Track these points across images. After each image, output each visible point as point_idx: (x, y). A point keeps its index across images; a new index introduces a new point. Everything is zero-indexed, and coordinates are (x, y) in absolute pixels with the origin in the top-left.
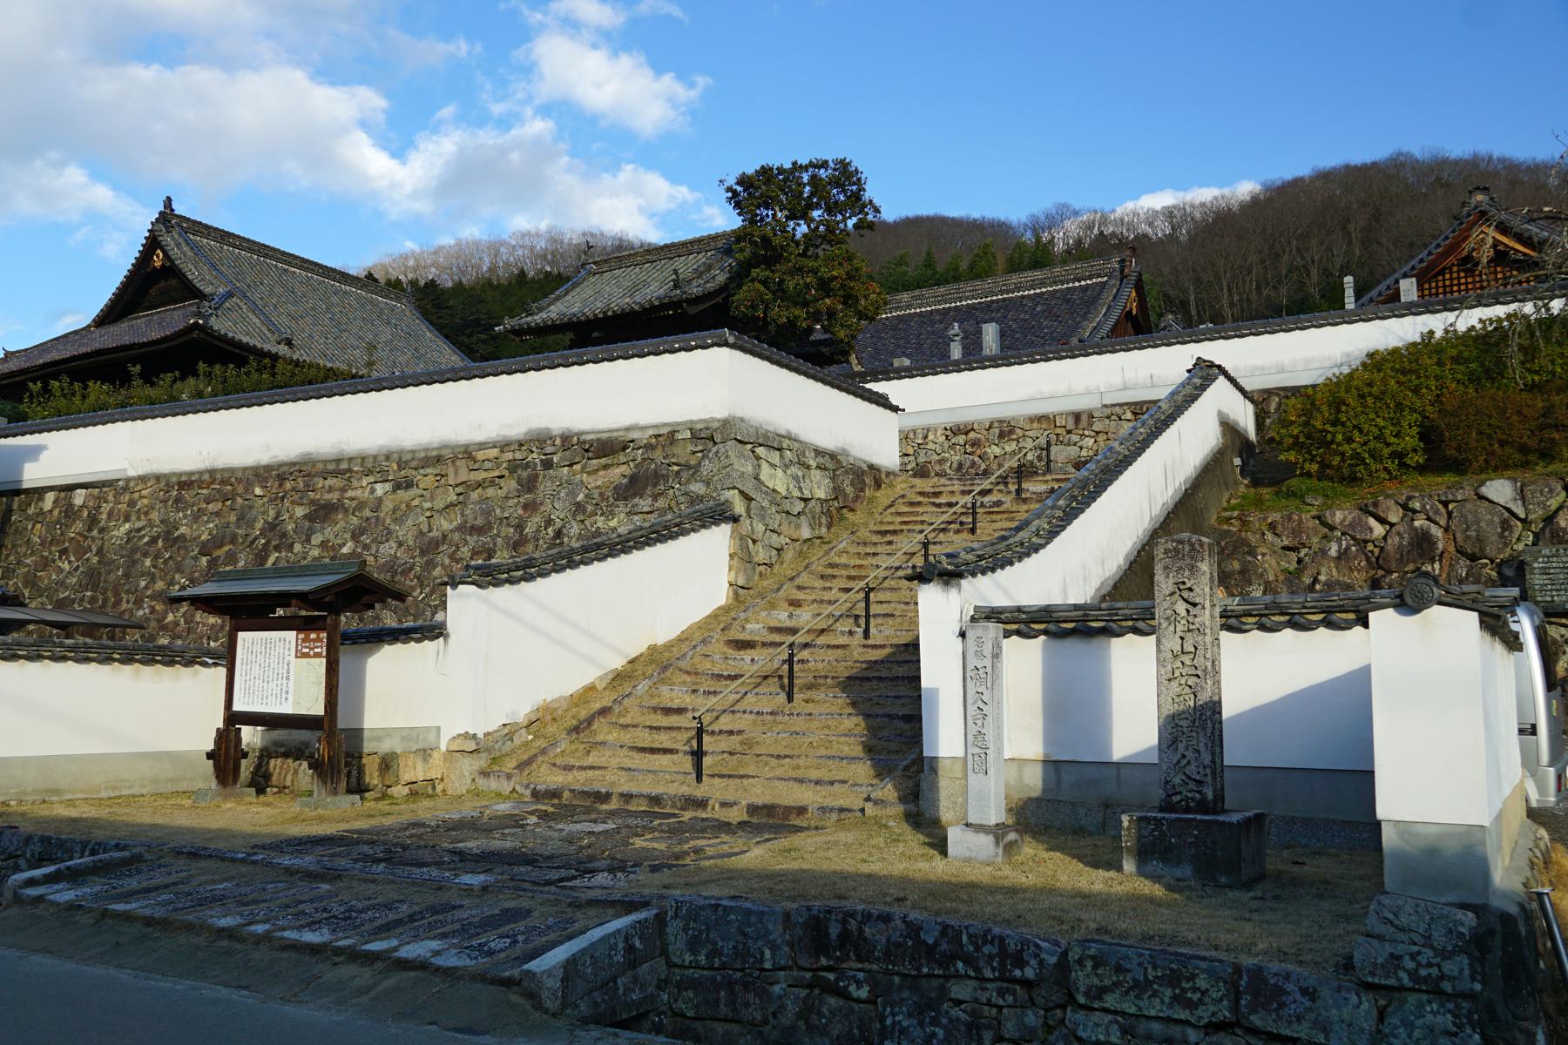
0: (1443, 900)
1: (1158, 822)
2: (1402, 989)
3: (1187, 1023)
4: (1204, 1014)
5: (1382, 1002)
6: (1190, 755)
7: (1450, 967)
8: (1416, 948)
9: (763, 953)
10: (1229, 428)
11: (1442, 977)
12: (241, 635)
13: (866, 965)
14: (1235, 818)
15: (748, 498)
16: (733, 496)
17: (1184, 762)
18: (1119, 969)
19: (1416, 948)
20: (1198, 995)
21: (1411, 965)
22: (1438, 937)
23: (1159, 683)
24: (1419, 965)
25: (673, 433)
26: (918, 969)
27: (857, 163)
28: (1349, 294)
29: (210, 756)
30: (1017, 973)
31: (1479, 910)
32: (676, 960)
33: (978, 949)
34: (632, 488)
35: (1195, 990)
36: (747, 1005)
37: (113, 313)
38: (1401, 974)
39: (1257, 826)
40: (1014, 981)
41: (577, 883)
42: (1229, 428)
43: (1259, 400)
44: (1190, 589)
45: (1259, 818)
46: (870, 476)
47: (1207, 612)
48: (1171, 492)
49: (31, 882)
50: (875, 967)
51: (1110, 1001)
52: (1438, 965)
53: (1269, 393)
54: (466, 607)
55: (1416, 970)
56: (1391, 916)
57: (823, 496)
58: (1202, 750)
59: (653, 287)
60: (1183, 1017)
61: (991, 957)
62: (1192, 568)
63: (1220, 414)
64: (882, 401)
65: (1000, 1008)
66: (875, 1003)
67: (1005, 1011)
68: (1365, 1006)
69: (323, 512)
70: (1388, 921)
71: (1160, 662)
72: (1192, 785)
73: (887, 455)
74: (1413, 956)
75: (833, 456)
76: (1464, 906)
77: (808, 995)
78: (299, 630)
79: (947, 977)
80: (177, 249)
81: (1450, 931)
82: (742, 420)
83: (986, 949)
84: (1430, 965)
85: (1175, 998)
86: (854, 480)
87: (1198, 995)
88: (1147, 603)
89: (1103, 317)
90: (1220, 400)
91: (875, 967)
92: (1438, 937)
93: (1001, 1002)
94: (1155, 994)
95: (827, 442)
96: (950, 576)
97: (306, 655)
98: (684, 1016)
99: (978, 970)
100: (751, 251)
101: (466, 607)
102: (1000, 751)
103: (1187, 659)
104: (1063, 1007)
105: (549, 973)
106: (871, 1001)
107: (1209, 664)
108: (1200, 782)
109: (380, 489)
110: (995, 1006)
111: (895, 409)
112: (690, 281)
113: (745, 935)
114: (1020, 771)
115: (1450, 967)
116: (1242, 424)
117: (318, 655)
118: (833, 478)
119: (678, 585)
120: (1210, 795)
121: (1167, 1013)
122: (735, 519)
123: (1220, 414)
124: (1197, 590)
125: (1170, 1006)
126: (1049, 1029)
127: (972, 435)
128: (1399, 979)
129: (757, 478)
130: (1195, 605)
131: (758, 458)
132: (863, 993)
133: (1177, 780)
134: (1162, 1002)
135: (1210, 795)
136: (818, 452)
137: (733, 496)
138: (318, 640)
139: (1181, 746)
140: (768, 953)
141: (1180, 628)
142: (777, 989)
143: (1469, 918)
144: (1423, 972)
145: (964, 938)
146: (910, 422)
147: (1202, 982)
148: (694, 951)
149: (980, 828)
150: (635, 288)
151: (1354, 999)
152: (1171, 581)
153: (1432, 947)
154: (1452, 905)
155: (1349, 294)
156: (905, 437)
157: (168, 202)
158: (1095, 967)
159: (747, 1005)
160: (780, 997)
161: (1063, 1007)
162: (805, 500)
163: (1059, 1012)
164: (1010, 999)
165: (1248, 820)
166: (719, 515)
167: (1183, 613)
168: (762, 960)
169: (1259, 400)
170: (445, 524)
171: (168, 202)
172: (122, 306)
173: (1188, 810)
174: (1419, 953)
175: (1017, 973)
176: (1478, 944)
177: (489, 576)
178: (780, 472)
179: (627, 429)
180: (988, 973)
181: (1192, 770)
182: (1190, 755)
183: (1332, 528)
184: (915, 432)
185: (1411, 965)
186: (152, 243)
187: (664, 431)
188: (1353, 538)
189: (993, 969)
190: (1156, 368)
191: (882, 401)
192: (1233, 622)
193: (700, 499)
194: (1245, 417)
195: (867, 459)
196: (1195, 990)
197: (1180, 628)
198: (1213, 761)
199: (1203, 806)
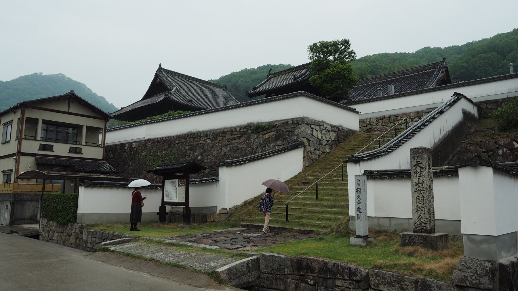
0: (482, 259)
2: (467, 287)
6: (422, 215)
7: (482, 280)
8: (472, 274)
10: (465, 113)
11: (480, 283)
12: (166, 181)
13: (313, 275)
14: (437, 234)
15: (309, 141)
16: (304, 140)
18: (384, 278)
19: (472, 274)
21: (470, 279)
22: (480, 271)
23: (412, 193)
24: (473, 280)
25: (287, 122)
26: (327, 276)
27: (312, 44)
29: (158, 213)
30: (355, 278)
31: (492, 262)
32: (263, 271)
33: (343, 270)
34: (278, 138)
36: (280, 285)
37: (147, 96)
38: (467, 282)
39: (428, 234)
40: (353, 280)
41: (240, 249)
42: (465, 113)
43: (478, 105)
44: (421, 163)
45: (446, 236)
46: (351, 132)
47: (427, 170)
48: (442, 135)
49: (106, 244)
50: (315, 275)
52: (479, 280)
54: (224, 173)
55: (472, 281)
56: (464, 264)
59: (288, 80)
61: (347, 273)
62: (422, 157)
63: (463, 110)
64: (354, 111)
65: (350, 288)
69: (193, 148)
70: (463, 265)
71: (412, 186)
72: (423, 224)
74: (471, 277)
75: (337, 127)
76: (489, 261)
78: (179, 179)
79: (335, 279)
80: (165, 77)
81: (483, 269)
82: (307, 118)
83: (346, 270)
84: (476, 279)
86: (343, 135)
89: (434, 81)
91: (315, 275)
92: (480, 271)
93: (350, 287)
94: (393, 286)
95: (336, 123)
96: (356, 161)
97: (181, 186)
98: (264, 287)
99: (343, 277)
100: (317, 66)
101: (224, 173)
102: (366, 213)
103: (420, 185)
105: (222, 272)
106: (314, 285)
108: (425, 224)
109: (208, 141)
111: (358, 113)
113: (280, 264)
114: (378, 220)
115: (482, 280)
116: (472, 112)
117: (184, 186)
118: (337, 134)
119: (288, 166)
120: (429, 228)
122: (305, 147)
123: (463, 110)
124: (423, 163)
128: (466, 284)
129: (312, 134)
130: (422, 168)
131: (312, 128)
132: (312, 282)
133: (418, 223)
135: (429, 228)
136: (332, 126)
137: (304, 140)
138: (184, 181)
139: (419, 212)
140: (286, 270)
142: (289, 280)
143: (489, 265)
144: (474, 282)
145: (340, 267)
146: (364, 117)
148: (267, 269)
149: (359, 237)
152: (415, 161)
153: (477, 274)
154: (485, 261)
156: (361, 121)
157: (160, 65)
158: (376, 277)
159: (280, 285)
160: (290, 283)
162: (328, 141)
164: (352, 286)
165: (441, 236)
166: (297, 145)
167: (419, 171)
168: (285, 272)
170: (225, 150)
171: (160, 65)
172: (149, 94)
173: (421, 232)
174: (473, 276)
175: (355, 278)
176: (491, 273)
177: (229, 165)
178: (319, 132)
180: (346, 278)
181: (423, 220)
182: (422, 215)
183: (500, 145)
184: (366, 119)
185: (470, 279)
186: (156, 77)
187: (285, 122)
188: (508, 149)
189: (348, 277)
190: (445, 96)
191: (354, 111)
192: (438, 175)
193: (295, 141)
194: (473, 110)
195: (349, 128)
198: (430, 217)
199: (427, 231)
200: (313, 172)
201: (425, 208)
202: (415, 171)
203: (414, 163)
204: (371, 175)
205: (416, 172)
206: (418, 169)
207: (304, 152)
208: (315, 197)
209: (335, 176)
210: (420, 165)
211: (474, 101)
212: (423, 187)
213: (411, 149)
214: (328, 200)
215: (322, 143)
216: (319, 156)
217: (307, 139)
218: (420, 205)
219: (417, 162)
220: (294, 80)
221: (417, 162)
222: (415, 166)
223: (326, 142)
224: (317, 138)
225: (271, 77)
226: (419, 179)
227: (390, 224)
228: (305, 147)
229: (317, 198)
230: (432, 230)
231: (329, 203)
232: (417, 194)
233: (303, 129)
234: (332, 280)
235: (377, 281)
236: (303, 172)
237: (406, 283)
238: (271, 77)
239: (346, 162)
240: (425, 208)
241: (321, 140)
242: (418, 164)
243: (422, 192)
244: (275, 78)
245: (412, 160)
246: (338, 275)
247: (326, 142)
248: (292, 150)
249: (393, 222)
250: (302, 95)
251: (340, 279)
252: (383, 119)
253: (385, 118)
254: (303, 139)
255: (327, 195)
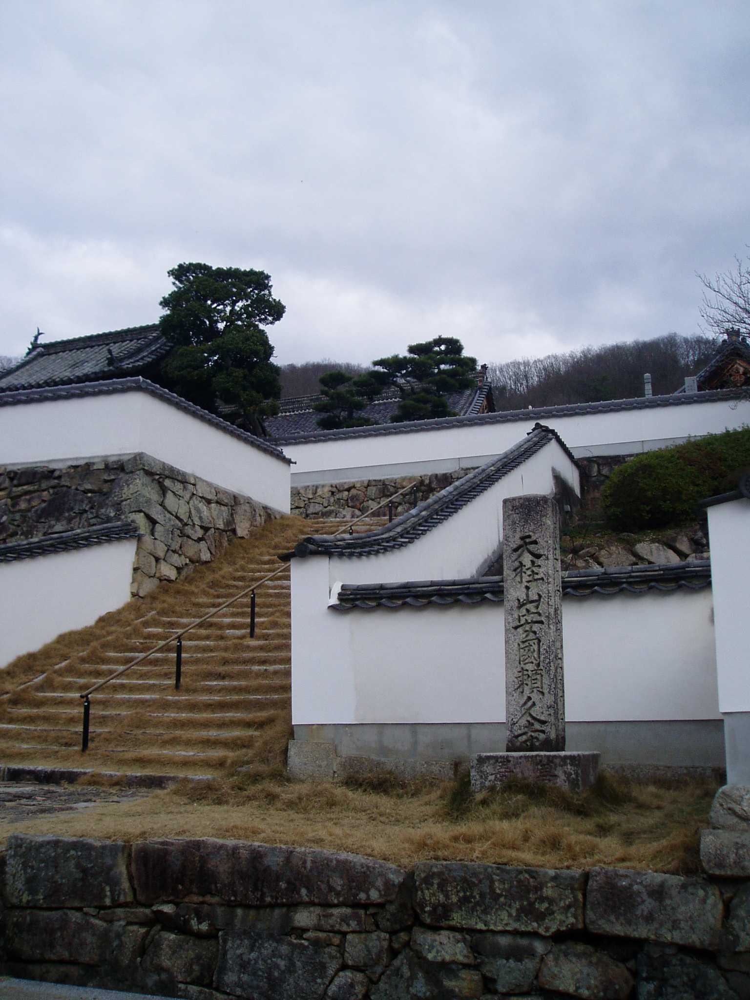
1: (507, 760)
3: (535, 935)
4: (553, 925)
5: (727, 895)
6: (535, 697)
9: (103, 890)
17: (530, 703)
20: (546, 905)
23: (506, 630)
28: (648, 387)
30: (362, 896)
32: (15, 901)
35: (542, 899)
43: (583, 465)
44: (535, 542)
51: (457, 918)
53: (590, 460)
57: (222, 526)
58: (546, 691)
60: (530, 929)
65: (344, 934)
66: (216, 937)
67: (349, 937)
68: (711, 900)
72: (537, 726)
73: (282, 504)
77: (147, 934)
85: (521, 910)
87: (546, 905)
88: (496, 578)
90: (550, 458)
93: (345, 928)
104: (408, 929)
107: (552, 611)
110: (339, 932)
111: (288, 462)
112: (121, 360)
120: (553, 736)
121: (513, 926)
122: (139, 538)
125: (517, 919)
126: (394, 953)
127: (353, 492)
130: (538, 556)
133: (523, 722)
134: (510, 915)
135: (553, 736)
139: (526, 688)
141: (526, 578)
147: (548, 892)
148: (32, 891)
150: (74, 366)
151: (701, 893)
152: (518, 535)
155: (648, 387)
161: (408, 929)
163: (403, 936)
166: (127, 532)
169: (583, 465)
173: (531, 749)
179: (49, 461)
182: (535, 697)
187: (82, 462)
193: (109, 520)
194: (572, 477)
196: (542, 899)
197: (526, 578)
199: (547, 745)
200: (163, 613)
201: (545, 676)
202: (517, 564)
203: (516, 541)
204: (355, 601)
205: (519, 568)
206: (527, 559)
207: (137, 553)
208: (172, 682)
209: (233, 626)
210: (532, 547)
211: (577, 455)
212: (540, 614)
213: (505, 501)
214: (210, 690)
215: (188, 530)
216: (179, 569)
217: (148, 517)
218: (530, 667)
219: (522, 538)
220: (109, 364)
221: (522, 538)
222: (516, 550)
223: (200, 533)
224: (177, 517)
225: (41, 355)
226: (527, 588)
227: (415, 743)
228: (139, 538)
229: (177, 686)
230: (559, 744)
231: (216, 698)
232: (521, 634)
233: (139, 487)
234: (277, 912)
235: (442, 898)
236: (128, 607)
237: (548, 892)
238: (41, 355)
239: (286, 558)
240: (545, 676)
241: (186, 525)
242: (526, 543)
243: (536, 627)
244: (53, 357)
245: (510, 533)
246: (304, 891)
247: (200, 533)
248: (99, 543)
249: (425, 738)
250: (138, 388)
251: (312, 904)
252: (348, 490)
253: (354, 487)
254: (133, 516)
255: (210, 675)
